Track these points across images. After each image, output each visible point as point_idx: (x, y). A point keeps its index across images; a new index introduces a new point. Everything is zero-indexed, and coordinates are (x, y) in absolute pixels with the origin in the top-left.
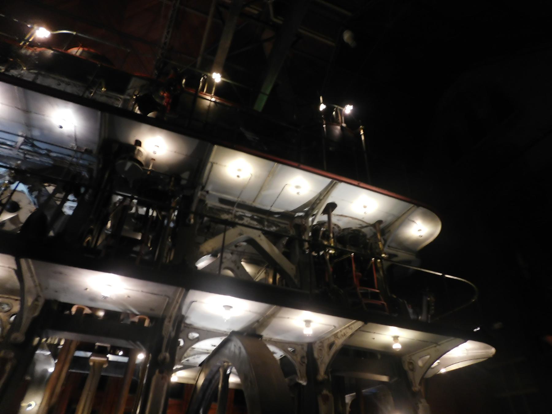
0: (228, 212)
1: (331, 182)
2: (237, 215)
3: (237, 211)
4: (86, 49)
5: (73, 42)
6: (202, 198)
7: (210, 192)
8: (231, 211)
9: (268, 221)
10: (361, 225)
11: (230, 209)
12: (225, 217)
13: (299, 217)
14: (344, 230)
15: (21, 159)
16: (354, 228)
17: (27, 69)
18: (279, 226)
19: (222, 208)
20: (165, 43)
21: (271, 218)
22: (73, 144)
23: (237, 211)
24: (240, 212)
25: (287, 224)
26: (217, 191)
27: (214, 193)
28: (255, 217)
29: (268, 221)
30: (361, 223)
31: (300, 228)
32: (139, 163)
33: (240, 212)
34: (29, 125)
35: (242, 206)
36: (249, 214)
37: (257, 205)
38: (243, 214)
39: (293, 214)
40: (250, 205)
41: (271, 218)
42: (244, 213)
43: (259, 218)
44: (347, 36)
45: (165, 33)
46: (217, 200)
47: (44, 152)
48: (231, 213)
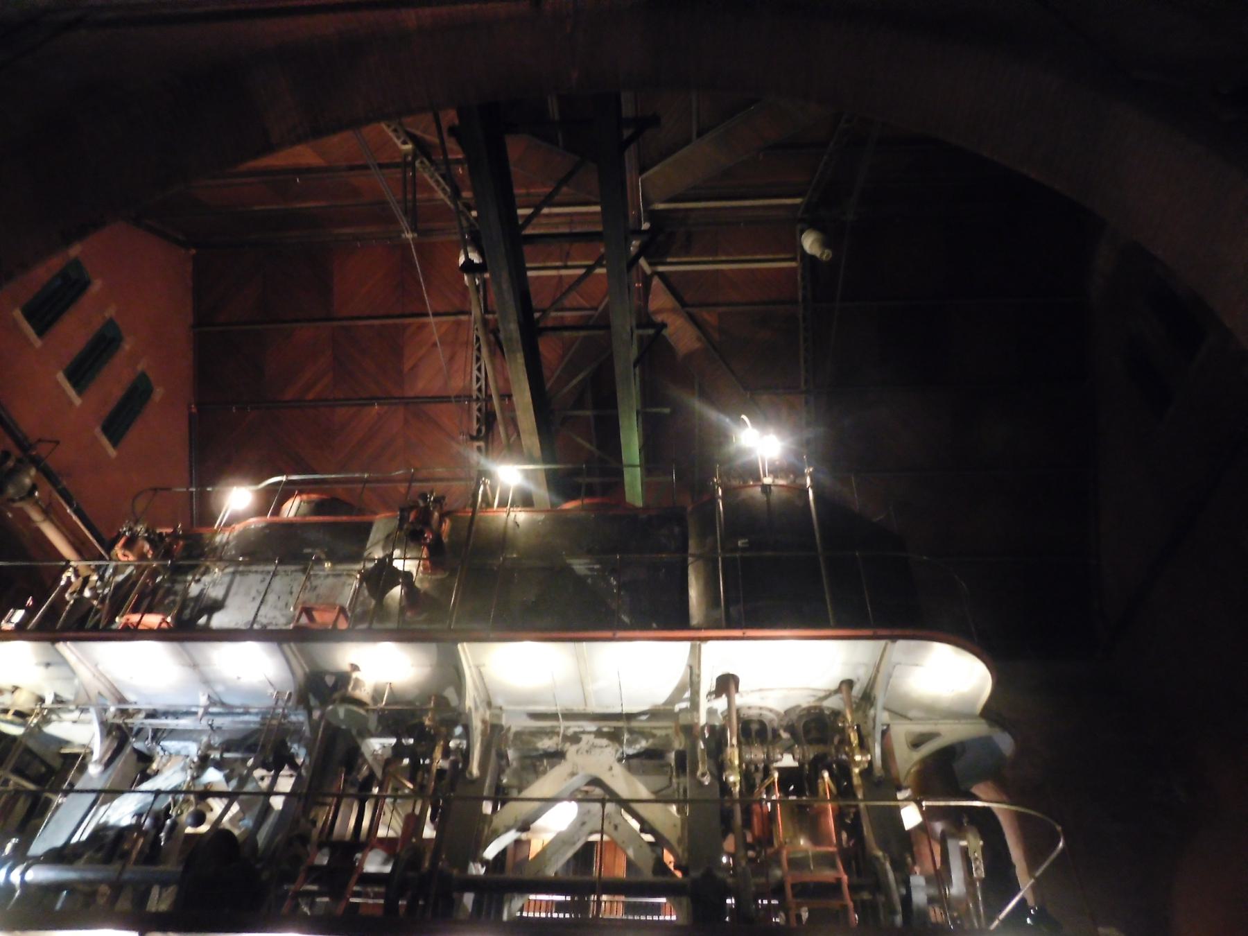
0: (552, 733)
1: (692, 647)
2: (569, 735)
3: (568, 728)
4: (305, 497)
5: (285, 493)
6: (495, 721)
7: (505, 707)
8: (557, 730)
9: (631, 731)
10: (814, 696)
11: (552, 727)
12: (546, 744)
13: (681, 710)
14: (787, 712)
15: (7, 874)
16: (805, 705)
17: (219, 570)
18: (654, 736)
19: (540, 727)
20: (479, 390)
21: (634, 724)
22: (271, 691)
23: (568, 728)
24: (574, 727)
25: (670, 727)
26: (519, 703)
27: (511, 708)
28: (605, 730)
29: (631, 731)
30: (814, 693)
31: (689, 730)
32: (359, 703)
33: (574, 727)
34: (206, 682)
35: (570, 716)
36: (591, 727)
37: (594, 707)
38: (582, 730)
39: (669, 707)
40: (583, 712)
41: (634, 724)
42: (582, 727)
43: (613, 730)
44: (810, 243)
45: (475, 373)
46: (525, 717)
47: (241, 710)
48: (558, 734)
